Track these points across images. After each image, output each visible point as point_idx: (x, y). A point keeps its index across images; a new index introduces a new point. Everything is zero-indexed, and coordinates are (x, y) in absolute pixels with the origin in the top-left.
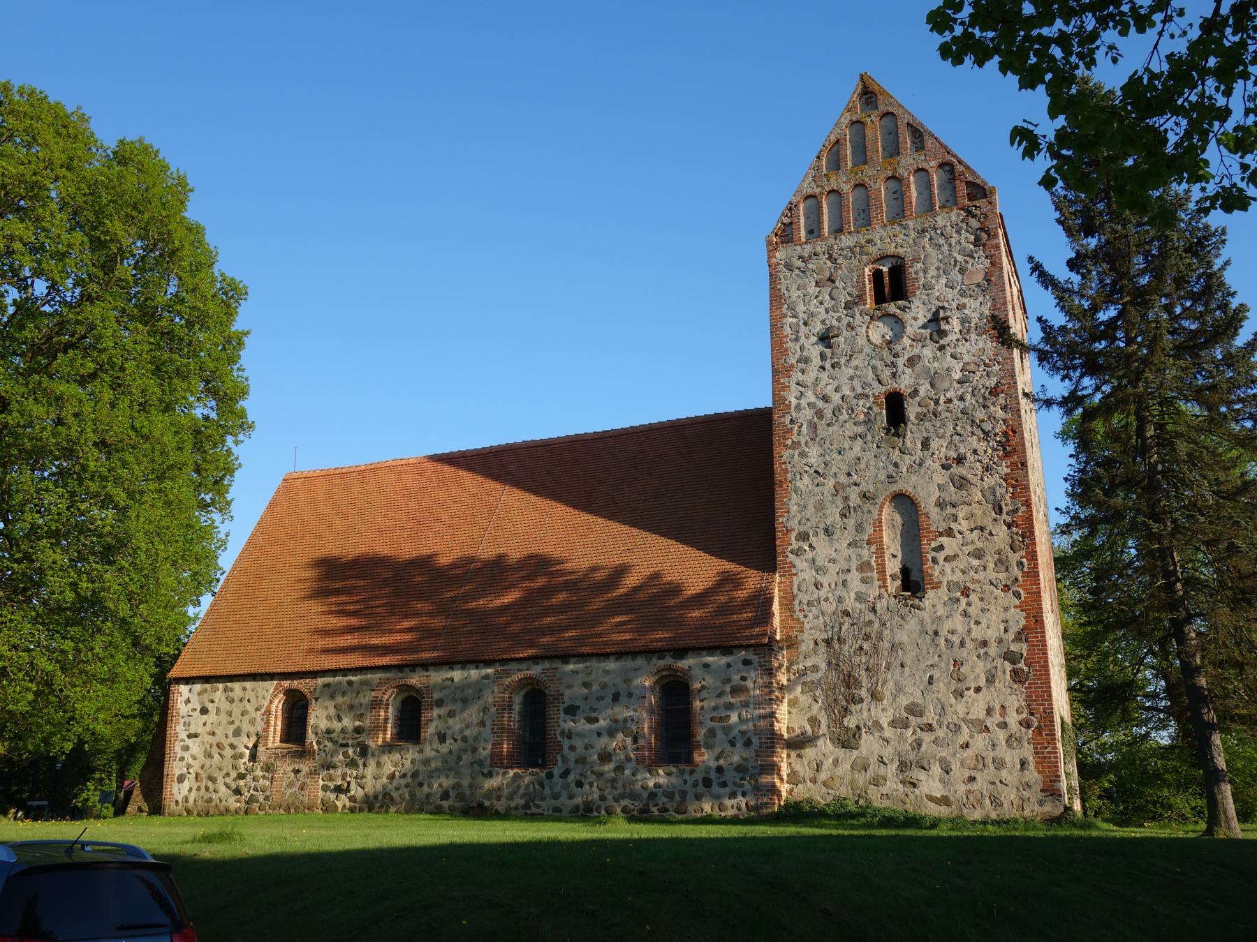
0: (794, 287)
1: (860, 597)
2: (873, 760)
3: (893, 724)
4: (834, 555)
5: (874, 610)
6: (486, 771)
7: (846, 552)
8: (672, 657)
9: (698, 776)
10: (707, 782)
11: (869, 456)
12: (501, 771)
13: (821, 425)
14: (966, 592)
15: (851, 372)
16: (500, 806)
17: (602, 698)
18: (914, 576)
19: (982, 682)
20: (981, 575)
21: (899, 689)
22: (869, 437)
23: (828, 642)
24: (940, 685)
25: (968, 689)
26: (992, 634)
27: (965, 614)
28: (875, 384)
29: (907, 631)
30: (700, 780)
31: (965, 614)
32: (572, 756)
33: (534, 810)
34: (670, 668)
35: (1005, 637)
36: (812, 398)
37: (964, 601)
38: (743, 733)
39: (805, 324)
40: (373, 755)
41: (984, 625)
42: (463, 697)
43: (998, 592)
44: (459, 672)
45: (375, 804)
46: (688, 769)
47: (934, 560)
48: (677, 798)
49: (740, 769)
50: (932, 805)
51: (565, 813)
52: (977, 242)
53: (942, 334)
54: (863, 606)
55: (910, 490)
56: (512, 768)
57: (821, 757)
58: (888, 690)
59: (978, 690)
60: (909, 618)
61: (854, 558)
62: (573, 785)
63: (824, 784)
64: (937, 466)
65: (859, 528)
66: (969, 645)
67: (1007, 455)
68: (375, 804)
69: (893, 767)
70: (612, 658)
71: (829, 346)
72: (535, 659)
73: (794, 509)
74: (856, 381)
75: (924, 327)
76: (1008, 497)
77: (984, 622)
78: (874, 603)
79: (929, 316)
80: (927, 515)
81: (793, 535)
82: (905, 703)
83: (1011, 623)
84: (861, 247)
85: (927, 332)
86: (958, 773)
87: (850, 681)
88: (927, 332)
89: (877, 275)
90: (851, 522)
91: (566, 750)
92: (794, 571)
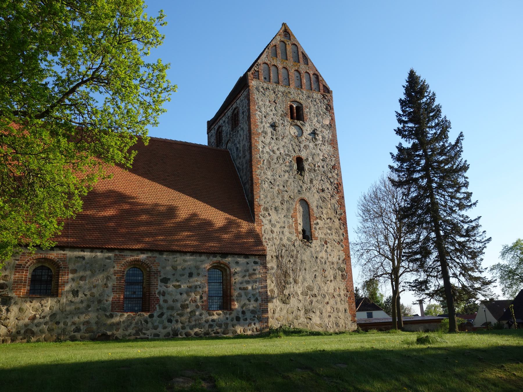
0: (260, 99)
1: (288, 239)
2: (295, 308)
3: (302, 293)
4: (278, 220)
5: (294, 245)
6: (108, 314)
7: (283, 219)
8: (221, 257)
9: (234, 315)
10: (238, 319)
11: (291, 180)
12: (119, 314)
13: (272, 163)
14: (326, 243)
15: (284, 144)
16: (119, 333)
17: (183, 275)
18: (308, 233)
19: (332, 278)
20: (330, 237)
21: (304, 279)
22: (291, 173)
23: (277, 257)
24: (319, 279)
25: (328, 281)
26: (335, 260)
27: (326, 251)
28: (293, 151)
29: (306, 255)
30: (235, 318)
31: (326, 251)
32: (165, 305)
33: (142, 336)
34: (219, 263)
35: (339, 261)
36: (268, 150)
37: (325, 246)
38: (254, 295)
39: (265, 117)
40: (16, 303)
41: (332, 256)
42: (93, 267)
43: (336, 244)
44: (89, 254)
45: (25, 334)
46: (229, 312)
47: (315, 228)
48: (223, 326)
49: (253, 312)
50: (317, 327)
51: (161, 337)
52: (326, 109)
53: (316, 139)
54: (290, 243)
55: (306, 199)
56: (127, 313)
57: (275, 307)
58: (300, 279)
59: (331, 281)
60: (307, 250)
61: (286, 222)
62: (166, 322)
63: (277, 319)
64: (315, 191)
65: (288, 210)
66: (328, 263)
67: (338, 192)
68: (25, 334)
69: (303, 312)
70: (188, 254)
71: (275, 130)
72: (142, 251)
73: (262, 196)
74: (285, 148)
75: (309, 134)
76: (339, 208)
77: (332, 255)
78: (294, 243)
79: (311, 131)
80: (313, 210)
81: (262, 207)
82: (306, 285)
83: (341, 256)
84: (286, 93)
85: (310, 137)
86: (325, 314)
87: (286, 274)
88: (310, 137)
89: (291, 107)
90: (285, 207)
91: (161, 302)
92: (262, 224)
